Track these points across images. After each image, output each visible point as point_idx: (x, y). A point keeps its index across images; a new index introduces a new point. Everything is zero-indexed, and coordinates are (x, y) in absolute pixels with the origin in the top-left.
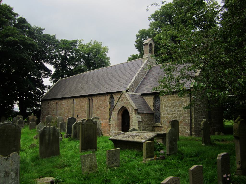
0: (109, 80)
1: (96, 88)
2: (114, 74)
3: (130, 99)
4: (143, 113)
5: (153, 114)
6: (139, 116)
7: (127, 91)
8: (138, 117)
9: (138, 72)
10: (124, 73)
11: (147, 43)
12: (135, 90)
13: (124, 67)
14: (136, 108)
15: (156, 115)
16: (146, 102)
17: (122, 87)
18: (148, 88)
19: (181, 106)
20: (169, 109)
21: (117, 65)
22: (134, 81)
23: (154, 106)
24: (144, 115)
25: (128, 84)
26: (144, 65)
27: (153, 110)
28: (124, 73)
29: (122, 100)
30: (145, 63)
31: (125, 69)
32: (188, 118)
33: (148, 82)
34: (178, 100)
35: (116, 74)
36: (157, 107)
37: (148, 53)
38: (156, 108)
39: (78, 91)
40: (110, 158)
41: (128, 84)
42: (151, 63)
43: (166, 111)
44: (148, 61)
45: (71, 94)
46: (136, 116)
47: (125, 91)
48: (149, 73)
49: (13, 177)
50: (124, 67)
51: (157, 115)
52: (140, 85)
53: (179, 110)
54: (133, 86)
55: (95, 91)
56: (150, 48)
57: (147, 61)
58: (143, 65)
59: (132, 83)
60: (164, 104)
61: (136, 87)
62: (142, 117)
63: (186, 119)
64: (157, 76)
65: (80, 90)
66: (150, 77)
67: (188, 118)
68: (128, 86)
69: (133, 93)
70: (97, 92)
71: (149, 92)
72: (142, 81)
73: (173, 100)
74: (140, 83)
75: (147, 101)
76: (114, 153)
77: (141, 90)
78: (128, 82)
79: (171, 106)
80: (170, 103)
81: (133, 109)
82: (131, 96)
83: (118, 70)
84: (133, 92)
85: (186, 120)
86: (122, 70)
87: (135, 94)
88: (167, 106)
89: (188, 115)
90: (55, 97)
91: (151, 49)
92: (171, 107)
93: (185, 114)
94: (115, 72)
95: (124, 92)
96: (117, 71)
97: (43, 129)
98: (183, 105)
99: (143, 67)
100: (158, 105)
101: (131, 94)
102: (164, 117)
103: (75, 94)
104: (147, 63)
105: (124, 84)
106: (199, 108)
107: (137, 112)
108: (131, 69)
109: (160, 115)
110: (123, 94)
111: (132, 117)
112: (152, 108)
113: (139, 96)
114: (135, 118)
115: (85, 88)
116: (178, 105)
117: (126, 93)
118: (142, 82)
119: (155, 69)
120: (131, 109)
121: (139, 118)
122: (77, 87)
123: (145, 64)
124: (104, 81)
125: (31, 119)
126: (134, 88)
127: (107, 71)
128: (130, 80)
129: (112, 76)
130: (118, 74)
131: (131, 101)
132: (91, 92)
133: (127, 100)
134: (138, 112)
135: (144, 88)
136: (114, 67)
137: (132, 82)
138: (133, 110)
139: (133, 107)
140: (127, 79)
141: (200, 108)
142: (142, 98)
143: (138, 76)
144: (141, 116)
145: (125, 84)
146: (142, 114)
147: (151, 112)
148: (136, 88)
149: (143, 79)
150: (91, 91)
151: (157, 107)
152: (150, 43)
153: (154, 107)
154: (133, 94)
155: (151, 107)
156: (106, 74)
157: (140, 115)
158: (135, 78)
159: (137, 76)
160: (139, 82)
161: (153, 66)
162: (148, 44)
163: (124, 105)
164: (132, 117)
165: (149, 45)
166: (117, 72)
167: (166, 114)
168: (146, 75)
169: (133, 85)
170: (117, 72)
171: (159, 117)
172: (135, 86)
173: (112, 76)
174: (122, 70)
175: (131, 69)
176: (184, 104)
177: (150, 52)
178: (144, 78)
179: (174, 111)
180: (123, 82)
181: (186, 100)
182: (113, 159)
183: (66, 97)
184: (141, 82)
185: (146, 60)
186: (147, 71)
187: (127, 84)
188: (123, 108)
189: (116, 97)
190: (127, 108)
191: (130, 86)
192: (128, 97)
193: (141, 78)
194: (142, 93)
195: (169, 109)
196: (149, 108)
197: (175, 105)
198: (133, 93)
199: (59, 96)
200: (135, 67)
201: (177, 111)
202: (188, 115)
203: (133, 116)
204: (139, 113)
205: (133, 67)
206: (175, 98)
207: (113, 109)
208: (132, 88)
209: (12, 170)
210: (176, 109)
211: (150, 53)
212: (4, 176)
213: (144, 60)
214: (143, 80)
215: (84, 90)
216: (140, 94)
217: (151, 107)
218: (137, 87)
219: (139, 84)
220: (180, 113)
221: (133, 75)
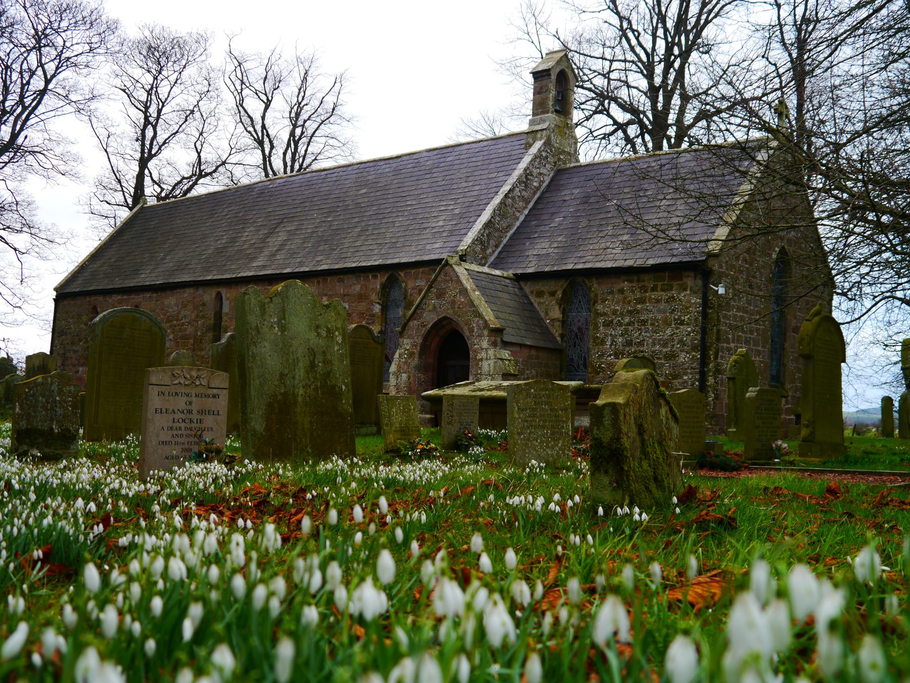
0: (381, 216)
1: (321, 248)
2: (401, 190)
3: (474, 291)
4: (522, 346)
5: (557, 351)
6: (506, 354)
7: (463, 258)
8: (502, 359)
9: (506, 188)
10: (446, 187)
11: (549, 70)
12: (492, 259)
13: (442, 165)
14: (494, 323)
15: (572, 360)
16: (534, 307)
17: (437, 246)
18: (544, 252)
19: (670, 325)
20: (622, 335)
21: (415, 156)
22: (488, 224)
23: (563, 322)
24: (526, 352)
25: (463, 232)
26: (531, 161)
27: (559, 339)
28: (446, 187)
29: (440, 295)
30: (534, 150)
31: (447, 173)
32: (692, 368)
33: (542, 228)
34: (658, 301)
35: (411, 193)
36: (575, 329)
37: (548, 112)
38: (571, 331)
39: (238, 260)
40: (452, 416)
41: (463, 232)
42: (560, 153)
43: (609, 343)
44: (548, 143)
45: (208, 270)
46: (495, 356)
47: (456, 259)
48: (547, 195)
49: (340, 342)
50: (442, 165)
51: (576, 359)
52: (511, 238)
53: (660, 340)
54: (482, 243)
55: (319, 258)
56: (558, 92)
57: (544, 144)
58: (527, 159)
59: (481, 230)
60: (605, 314)
61: (497, 246)
62: (516, 362)
63: (686, 374)
64: (580, 207)
65: (248, 252)
66: (553, 210)
67: (692, 368)
68: (465, 240)
69: (486, 269)
70: (329, 261)
71: (547, 269)
72: (518, 224)
73: (641, 301)
74: (512, 232)
75: (536, 305)
76: (464, 406)
77: (513, 260)
78: (465, 226)
79: (629, 324)
80: (628, 311)
81: (485, 328)
82: (475, 277)
83: (420, 177)
84: (483, 265)
85: (685, 378)
86: (435, 175)
87: (493, 273)
88: (615, 321)
89: (693, 356)
90: (132, 283)
91: (562, 97)
92: (631, 328)
93: (683, 355)
94: (406, 184)
95: (452, 261)
96: (414, 178)
97: (228, 341)
98: (675, 320)
99: (525, 170)
100: (579, 321)
101: (478, 272)
102: (599, 365)
103: (226, 271)
104: (544, 154)
105: (445, 234)
106: (733, 334)
107: (499, 340)
108: (476, 173)
109: (585, 358)
110: (447, 268)
111: (481, 360)
112: (556, 332)
113: (508, 281)
114: (492, 362)
115: (270, 244)
116: (657, 321)
117: (461, 264)
118: (518, 228)
119: (575, 180)
120: (478, 326)
121: (507, 362)
122: (233, 240)
123: (536, 157)
124: (356, 220)
125: (34, 368)
126: (489, 251)
127: (370, 178)
128: (472, 220)
129: (391, 201)
130: (420, 192)
131: (476, 295)
132: (301, 264)
133: (464, 291)
134: (504, 340)
135: (527, 254)
136: (399, 160)
137: (480, 227)
138: (486, 332)
139: (486, 321)
140: (457, 211)
141: (740, 334)
142: (516, 290)
143: (503, 203)
144: (513, 354)
145: (452, 233)
146: (518, 349)
147: (550, 346)
148: (496, 253)
149: (522, 218)
150: (299, 260)
151: (575, 329)
152: (558, 70)
153: (563, 327)
154: (485, 273)
155: (553, 325)
156: (364, 191)
157: (511, 351)
158: (494, 211)
159: (501, 203)
160: (509, 227)
161: (568, 165)
162: (550, 75)
163: (450, 313)
164: (481, 360)
165: (553, 77)
166: (413, 183)
167: (610, 355)
168: (536, 203)
169: (485, 238)
170: (413, 183)
171: (582, 367)
172: (492, 242)
173: (391, 201)
174: (435, 175)
175: (476, 173)
176: (680, 317)
177: (558, 108)
178: (526, 212)
179: (639, 342)
180: (441, 223)
181: (689, 301)
182: (460, 422)
183: (184, 280)
184: (515, 228)
185: (541, 139)
186: (540, 186)
187: (457, 233)
188: (445, 323)
189: (415, 284)
190: (462, 324)
191: (473, 243)
192: (468, 284)
193: (518, 214)
194: (520, 271)
195: (622, 335)
196: (545, 332)
197: (647, 321)
198: (486, 269)
199: (146, 278)
200: (492, 166)
201: (654, 344)
202: (693, 356)
203: (483, 355)
204: (506, 344)
205: (484, 167)
206: (648, 294)
207: (404, 328)
208: (478, 248)
209: (337, 329)
210: (648, 335)
211: (556, 111)
212: (327, 336)
213: (531, 141)
214: (524, 221)
215: (266, 252)
216: (510, 273)
217: (553, 325)
218: (499, 249)
219: (509, 234)
220: (665, 350)
221: (482, 197)
